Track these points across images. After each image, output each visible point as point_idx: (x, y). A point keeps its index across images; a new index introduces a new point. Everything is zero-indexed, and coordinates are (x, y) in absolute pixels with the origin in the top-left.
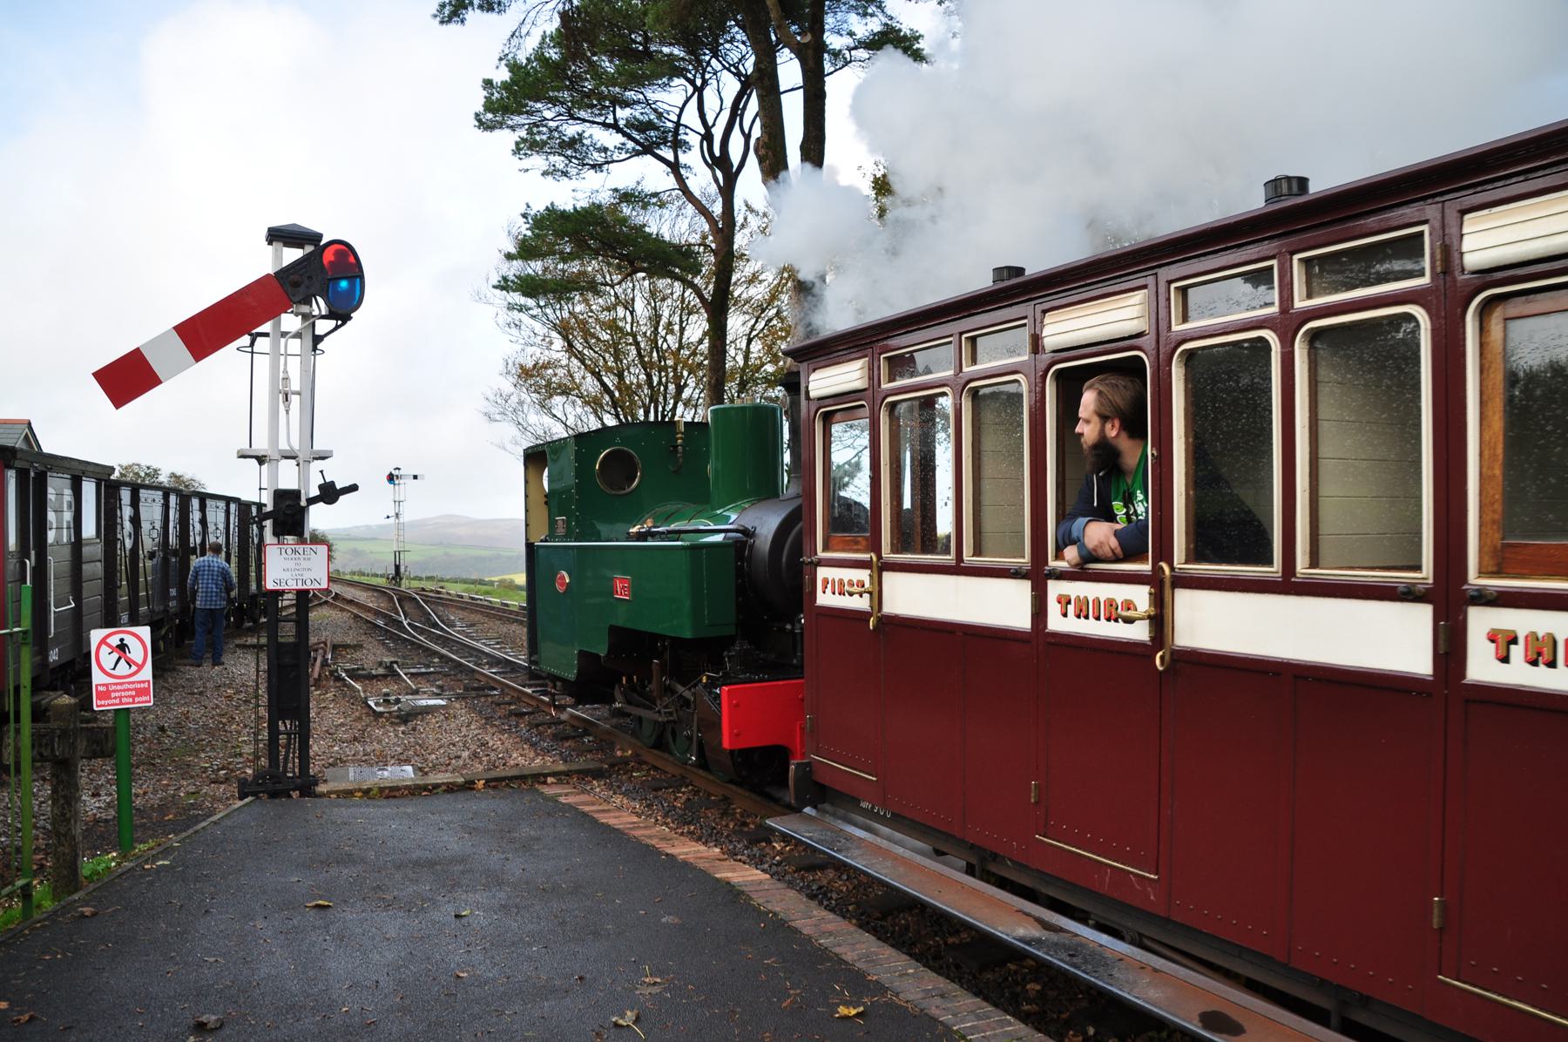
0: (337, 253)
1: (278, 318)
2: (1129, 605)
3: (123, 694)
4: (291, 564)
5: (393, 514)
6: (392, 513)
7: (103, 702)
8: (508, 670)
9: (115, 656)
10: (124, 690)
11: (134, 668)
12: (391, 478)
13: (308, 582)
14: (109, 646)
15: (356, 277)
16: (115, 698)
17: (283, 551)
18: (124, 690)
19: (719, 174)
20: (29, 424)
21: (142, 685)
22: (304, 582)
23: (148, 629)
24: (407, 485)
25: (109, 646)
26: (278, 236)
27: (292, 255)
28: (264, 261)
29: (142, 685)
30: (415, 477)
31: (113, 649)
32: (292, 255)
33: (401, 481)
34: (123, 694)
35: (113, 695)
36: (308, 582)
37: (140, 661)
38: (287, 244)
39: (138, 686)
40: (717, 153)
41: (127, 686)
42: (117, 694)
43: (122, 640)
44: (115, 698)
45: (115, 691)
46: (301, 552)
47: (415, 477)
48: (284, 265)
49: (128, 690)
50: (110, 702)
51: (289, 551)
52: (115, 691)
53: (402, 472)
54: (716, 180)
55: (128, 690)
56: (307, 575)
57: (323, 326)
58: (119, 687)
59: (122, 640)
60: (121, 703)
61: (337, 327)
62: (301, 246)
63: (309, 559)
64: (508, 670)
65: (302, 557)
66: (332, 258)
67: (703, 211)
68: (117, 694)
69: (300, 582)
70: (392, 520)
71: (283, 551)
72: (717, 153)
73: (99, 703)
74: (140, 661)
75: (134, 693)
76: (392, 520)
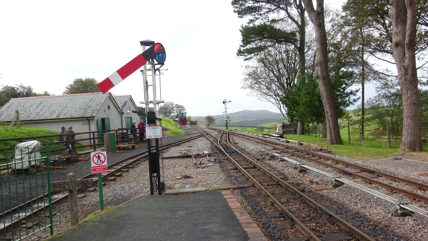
0: (159, 46)
1: (145, 65)
2: (21, 183)
3: (100, 169)
4: (152, 132)
5: (225, 111)
6: (225, 111)
7: (94, 172)
8: (223, 155)
9: (97, 159)
10: (100, 168)
11: (102, 162)
12: (224, 102)
13: (157, 136)
14: (96, 156)
15: (164, 53)
16: (98, 171)
17: (150, 128)
18: (100, 168)
19: (299, 10)
20: (131, 96)
21: (105, 167)
22: (156, 136)
23: (106, 152)
24: (228, 104)
25: (96, 156)
26: (143, 43)
27: (147, 48)
28: (140, 50)
29: (105, 167)
30: (230, 102)
31: (97, 157)
32: (147, 48)
33: (226, 103)
34: (100, 169)
35: (97, 170)
36: (157, 136)
37: (103, 161)
38: (146, 45)
39: (104, 167)
40: (298, 4)
41: (100, 167)
42: (98, 170)
43: (98, 155)
44: (98, 171)
45: (97, 169)
46: (155, 128)
47: (230, 102)
48: (146, 50)
49: (101, 168)
50: (96, 172)
51: (152, 128)
52: (97, 169)
53: (226, 101)
54: (298, 12)
55: (101, 168)
56: (157, 134)
57: (157, 67)
58: (98, 168)
59: (98, 155)
60: (99, 172)
61: (161, 67)
62: (149, 45)
63: (157, 130)
64: (223, 155)
65: (155, 129)
66: (157, 48)
67: (296, 22)
68: (98, 170)
69: (155, 136)
70: (225, 113)
71: (150, 128)
72: (298, 4)
73: (93, 172)
74: (103, 161)
75: (103, 169)
76: (225, 113)
